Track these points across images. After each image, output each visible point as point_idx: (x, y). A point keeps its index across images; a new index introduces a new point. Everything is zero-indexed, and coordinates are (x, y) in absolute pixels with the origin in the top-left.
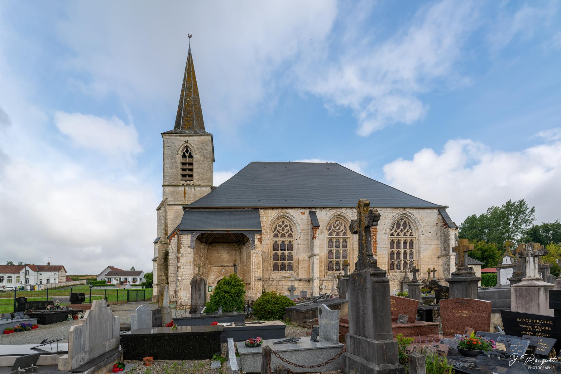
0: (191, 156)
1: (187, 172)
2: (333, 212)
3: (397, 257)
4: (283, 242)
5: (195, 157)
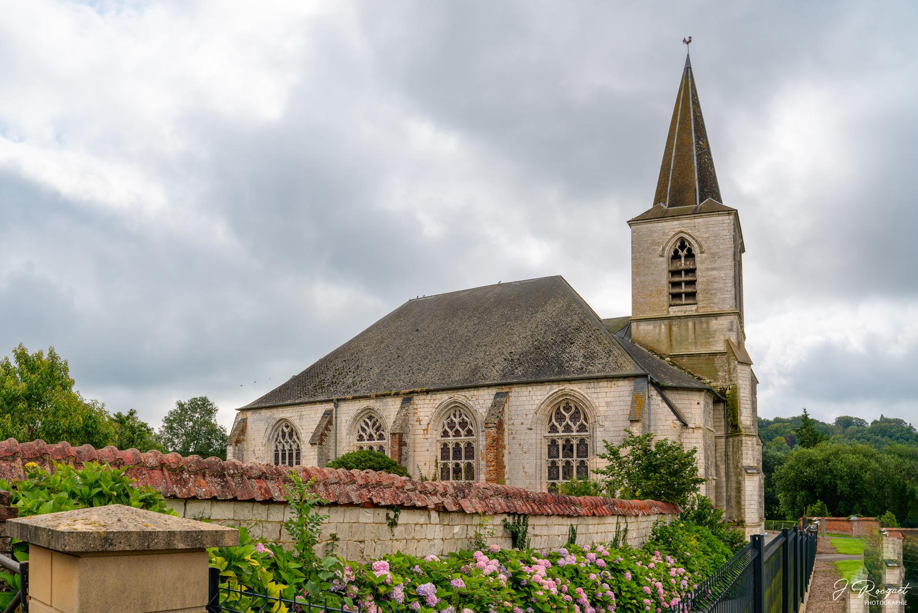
0: (690, 255)
1: (684, 289)
2: (445, 397)
3: (564, 473)
4: (457, 444)
5: (699, 257)
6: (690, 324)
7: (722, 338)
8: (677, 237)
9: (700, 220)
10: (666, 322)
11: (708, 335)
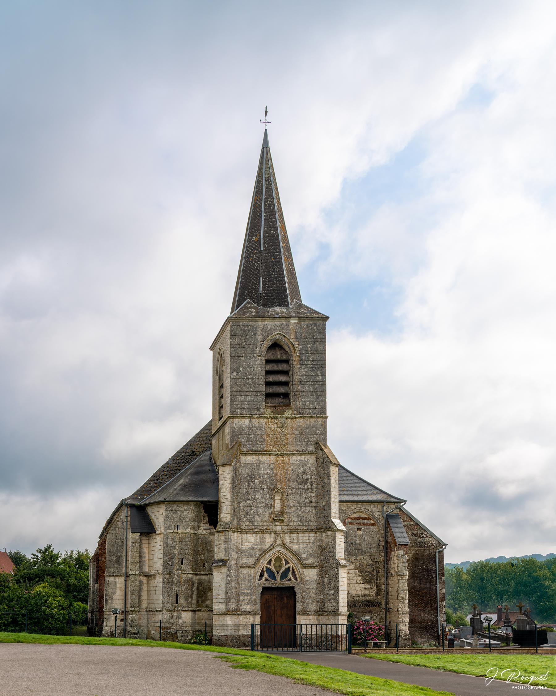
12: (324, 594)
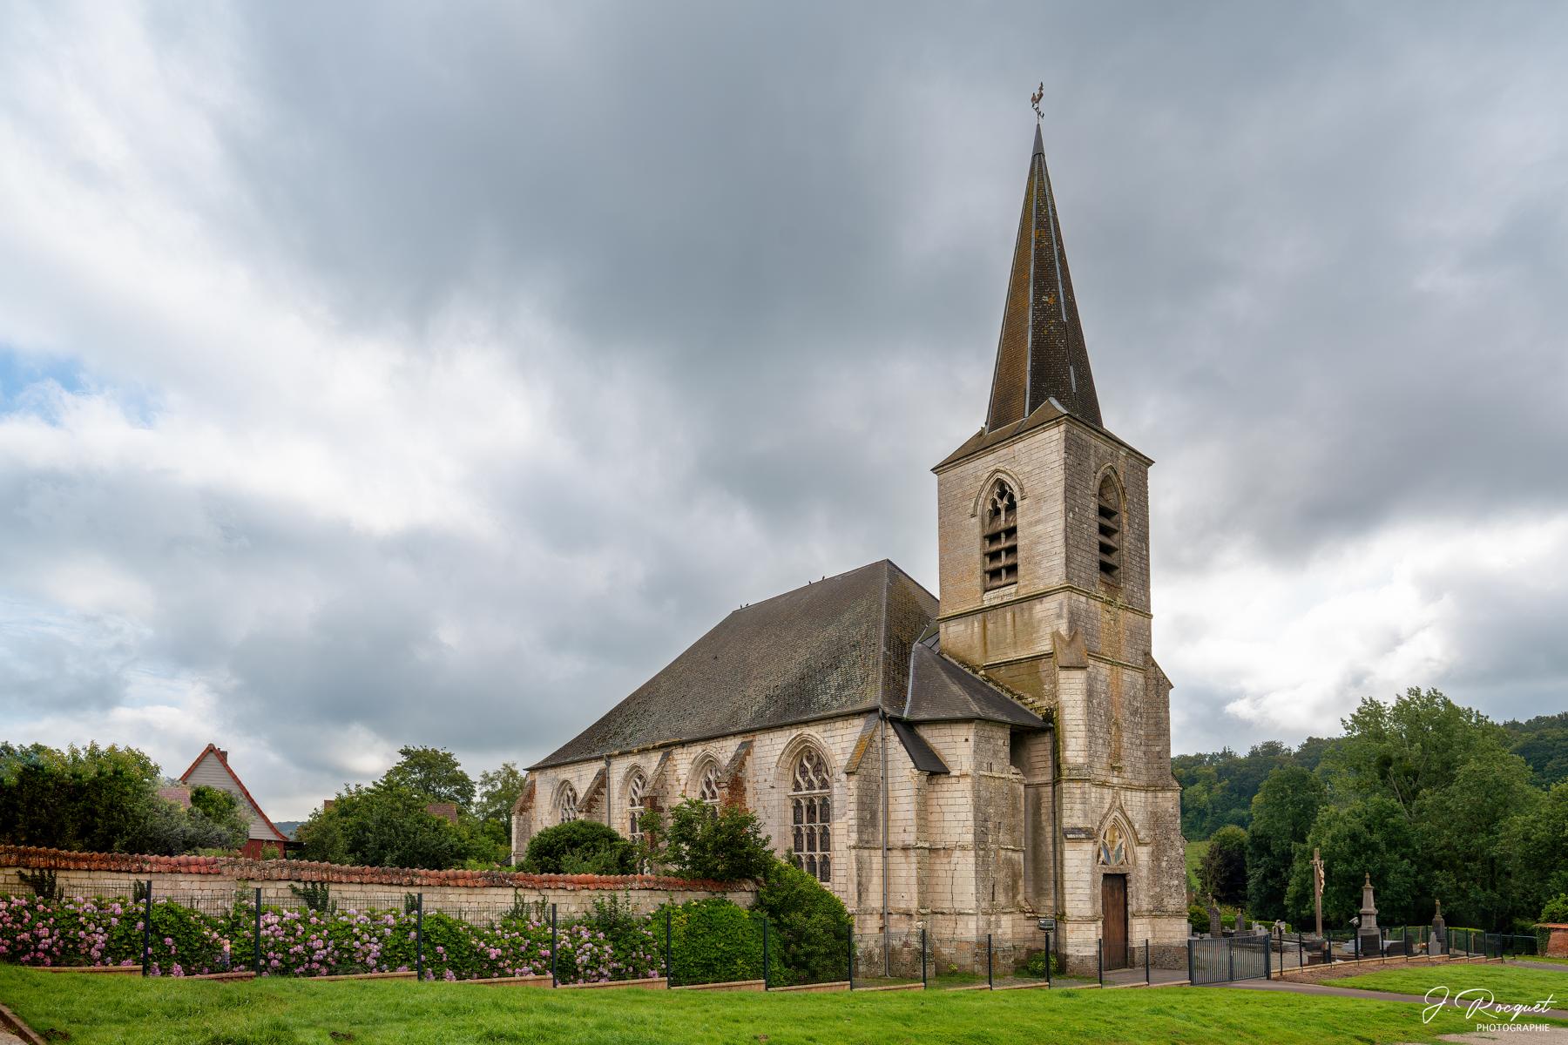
2: (698, 750)
6: (1009, 616)
7: (1049, 630)
8: (992, 481)
9: (1021, 445)
10: (980, 616)
11: (1031, 628)
12: (1162, 886)
